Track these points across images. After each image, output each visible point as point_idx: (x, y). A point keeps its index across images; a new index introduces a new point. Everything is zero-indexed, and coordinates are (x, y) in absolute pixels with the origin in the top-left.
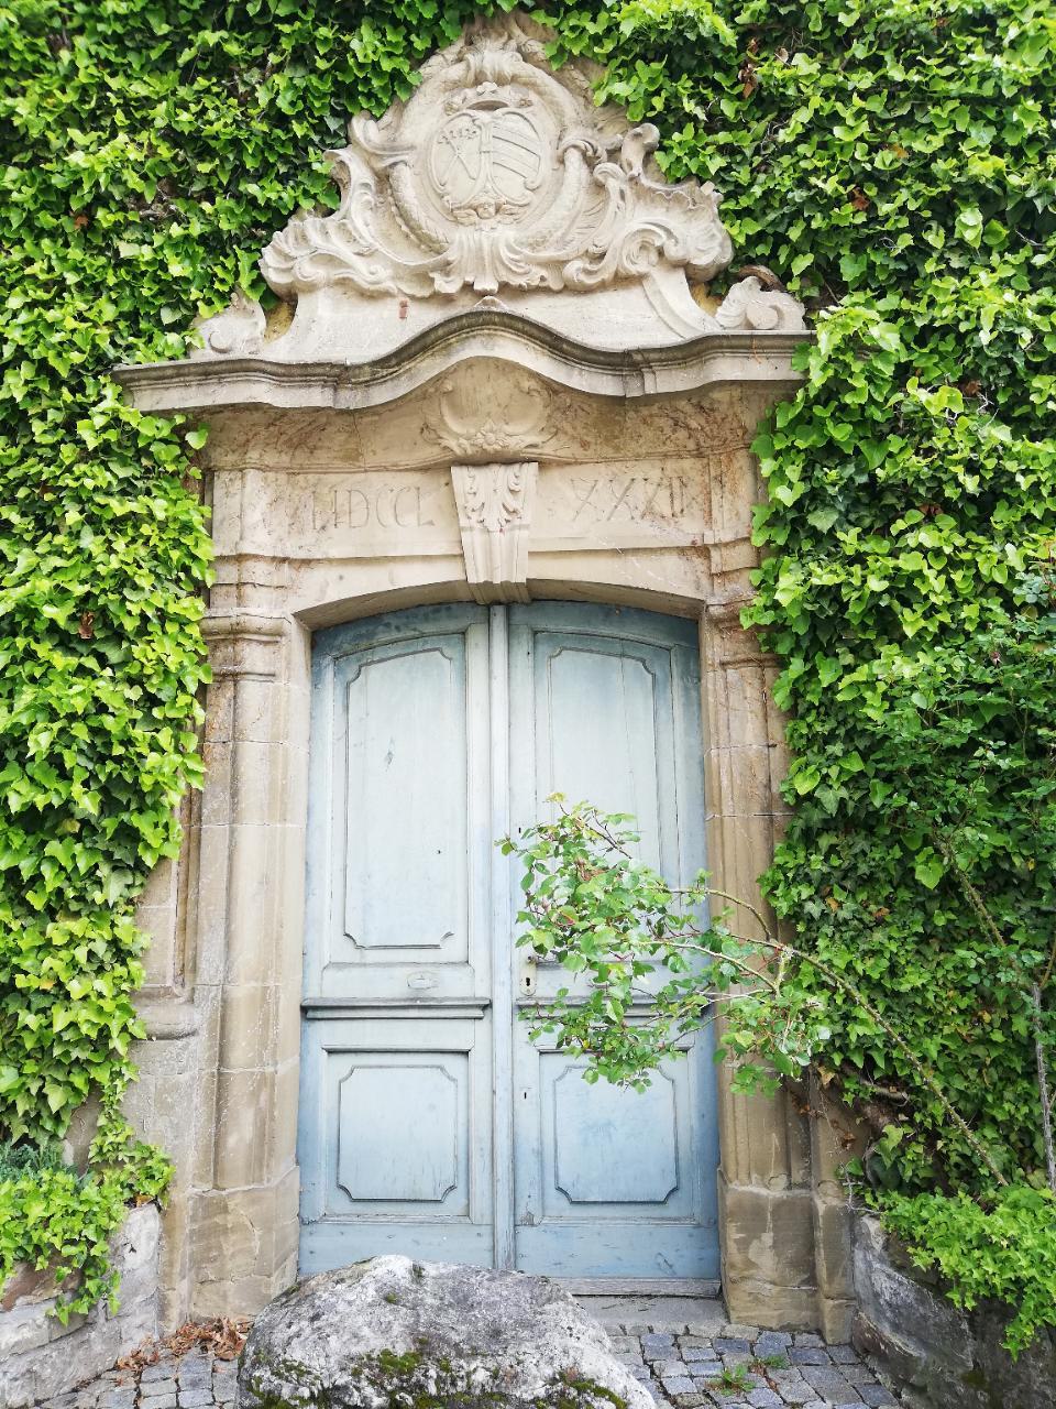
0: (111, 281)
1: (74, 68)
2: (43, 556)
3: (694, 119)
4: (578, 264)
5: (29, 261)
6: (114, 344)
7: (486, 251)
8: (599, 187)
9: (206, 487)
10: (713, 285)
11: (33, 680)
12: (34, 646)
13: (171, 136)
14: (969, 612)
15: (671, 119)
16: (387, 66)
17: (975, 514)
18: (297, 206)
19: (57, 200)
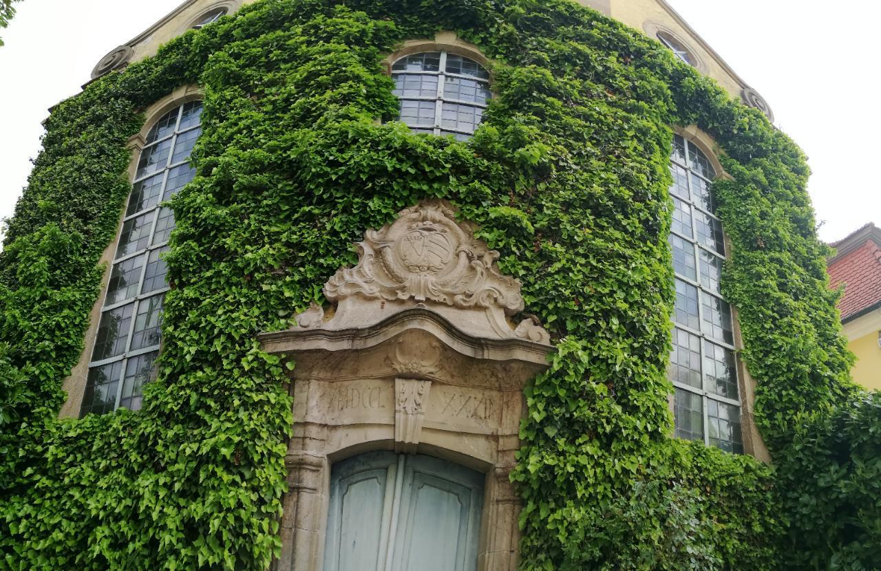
0: (258, 300)
1: (249, 225)
2: (222, 422)
3: (515, 254)
4: (461, 297)
5: (226, 296)
6: (258, 325)
7: (422, 284)
8: (472, 269)
9: (290, 389)
10: (514, 318)
11: (213, 487)
12: (216, 469)
13: (288, 244)
14: (600, 489)
15: (505, 251)
16: (384, 211)
17: (607, 441)
18: (340, 265)
19: (239, 271)
